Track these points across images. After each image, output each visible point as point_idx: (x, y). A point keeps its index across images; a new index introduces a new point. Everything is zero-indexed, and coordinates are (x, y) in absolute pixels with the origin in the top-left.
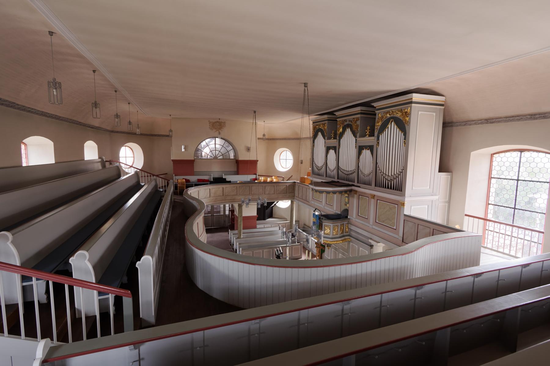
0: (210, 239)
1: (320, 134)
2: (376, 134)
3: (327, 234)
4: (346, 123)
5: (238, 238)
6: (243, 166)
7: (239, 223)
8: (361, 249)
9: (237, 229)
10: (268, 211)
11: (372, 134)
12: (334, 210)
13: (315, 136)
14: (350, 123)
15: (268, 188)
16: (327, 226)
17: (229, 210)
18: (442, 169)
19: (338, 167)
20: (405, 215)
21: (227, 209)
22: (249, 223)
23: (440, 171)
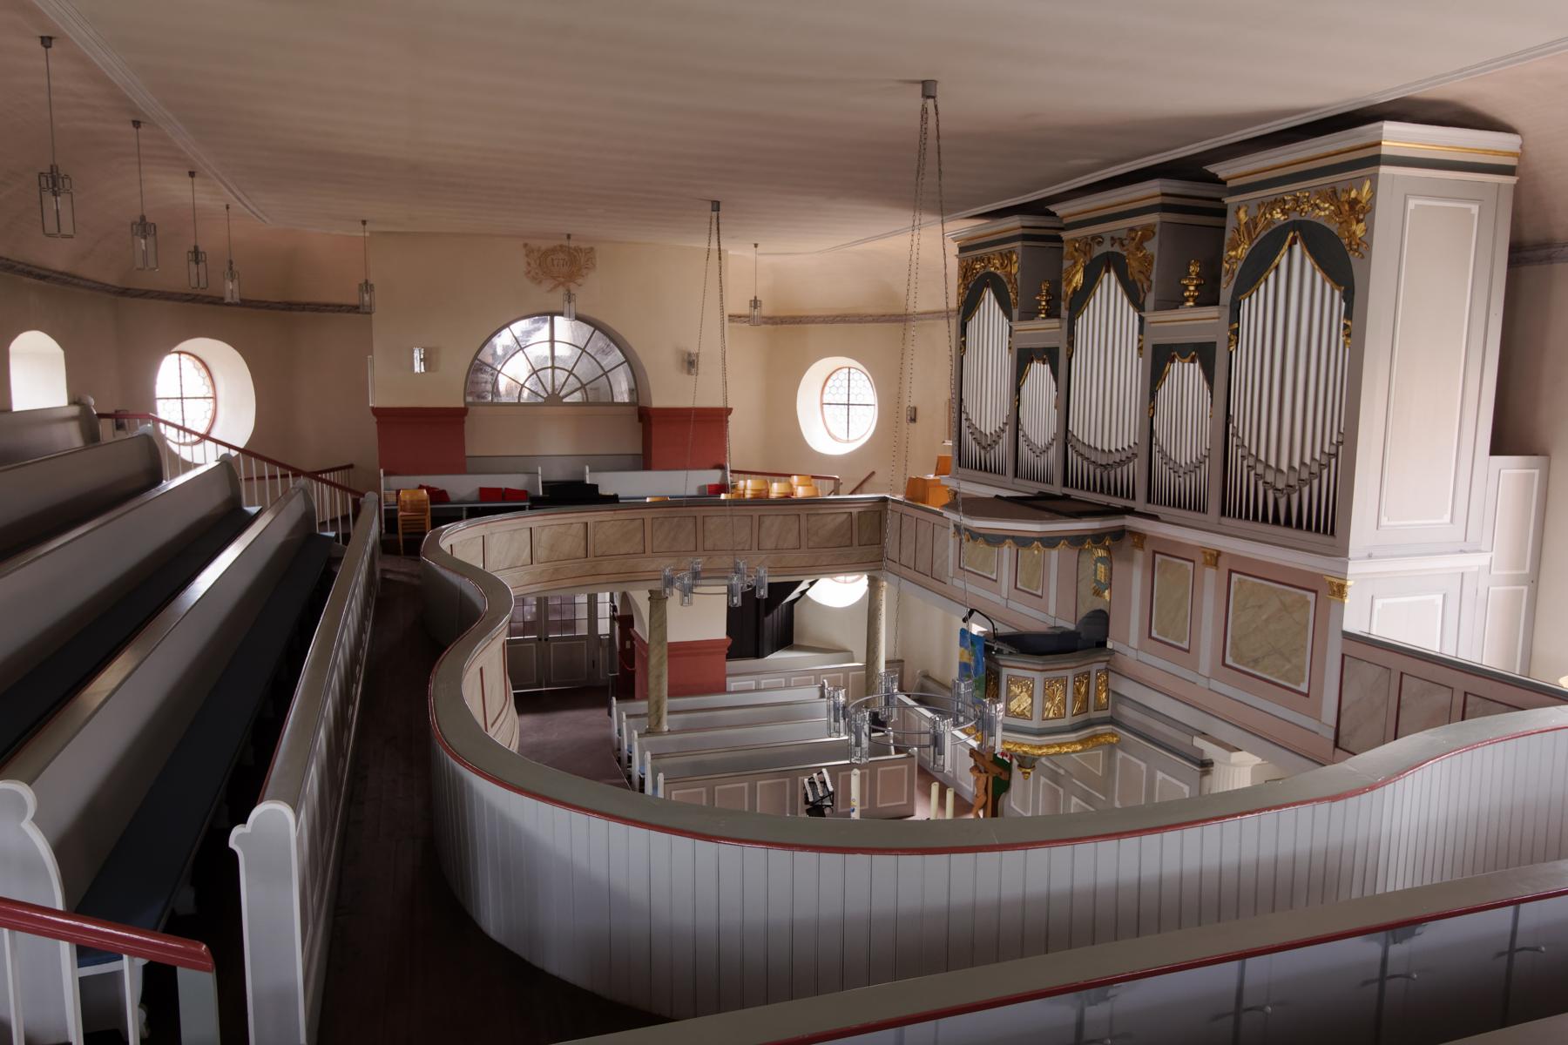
0: (534, 738)
1: (989, 296)
2: (1226, 294)
4: (1098, 251)
5: (649, 732)
8: (1160, 775)
9: (645, 697)
10: (772, 620)
11: (1208, 297)
12: (1050, 612)
14: (1117, 248)
15: (774, 524)
16: (1013, 680)
17: (613, 619)
18: (1500, 446)
19: (1065, 435)
20: (1348, 636)
21: (604, 610)
22: (696, 670)
23: (1496, 449)
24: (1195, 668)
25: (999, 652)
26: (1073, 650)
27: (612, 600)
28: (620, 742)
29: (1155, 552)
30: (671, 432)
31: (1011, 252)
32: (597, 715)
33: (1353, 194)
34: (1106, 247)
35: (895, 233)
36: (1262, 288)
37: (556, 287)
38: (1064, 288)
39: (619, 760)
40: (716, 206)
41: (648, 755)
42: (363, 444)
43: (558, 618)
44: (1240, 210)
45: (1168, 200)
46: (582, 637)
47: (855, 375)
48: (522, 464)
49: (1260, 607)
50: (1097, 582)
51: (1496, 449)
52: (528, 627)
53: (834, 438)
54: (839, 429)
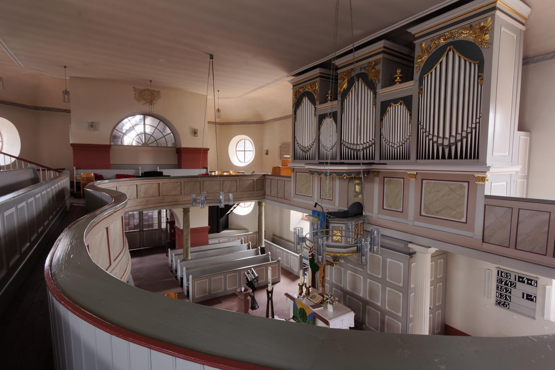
0: (138, 266)
1: (306, 100)
2: (416, 76)
3: (337, 241)
4: (353, 74)
5: (184, 260)
6: (184, 156)
7: (185, 238)
8: (389, 260)
9: (181, 247)
10: (222, 220)
11: (407, 77)
12: (338, 204)
13: (297, 104)
14: (363, 71)
15: (227, 184)
16: (334, 228)
17: (167, 223)
18: (520, 129)
19: (341, 142)
20: (487, 197)
21: (164, 220)
22: (199, 237)
23: (519, 130)
24: (406, 218)
25: (330, 217)
26: (347, 217)
27: (166, 216)
28: (172, 264)
29: (384, 177)
30: (187, 155)
31: (315, 82)
32: (163, 255)
33: (482, 24)
34: (358, 71)
35: (268, 84)
36: (438, 66)
37: (146, 103)
38: (339, 89)
39: (172, 271)
40: (212, 57)
41: (184, 268)
42: (67, 157)
43: (147, 223)
44: (421, 45)
45: (386, 50)
47: (247, 141)
48: (134, 167)
49: (439, 191)
50: (356, 192)
51: (519, 130)
52: (135, 227)
53: (240, 161)
54: (241, 158)
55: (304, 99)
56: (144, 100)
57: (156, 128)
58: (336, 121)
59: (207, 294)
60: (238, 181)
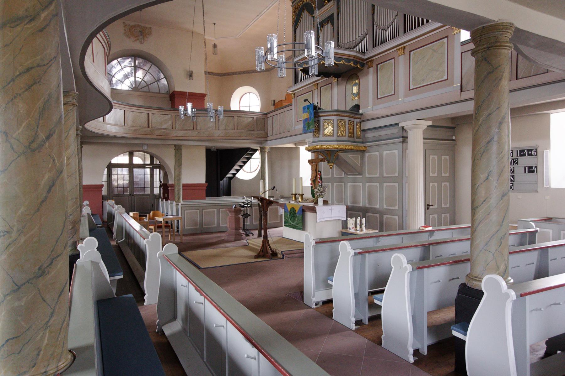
10: (223, 182)
17: (160, 187)
21: (157, 184)
37: (136, 40)
43: (138, 187)
46: (147, 195)
55: (303, 15)
56: (135, 37)
57: (148, 71)
58: (333, 25)
59: (198, 227)
60: (236, 118)
